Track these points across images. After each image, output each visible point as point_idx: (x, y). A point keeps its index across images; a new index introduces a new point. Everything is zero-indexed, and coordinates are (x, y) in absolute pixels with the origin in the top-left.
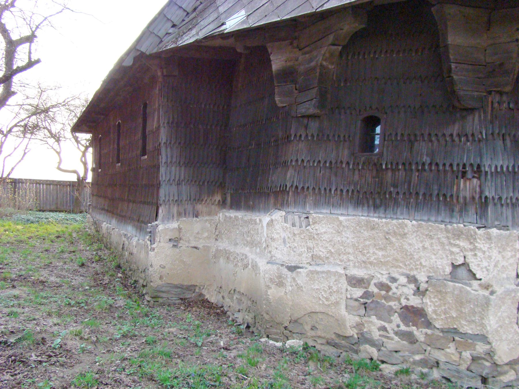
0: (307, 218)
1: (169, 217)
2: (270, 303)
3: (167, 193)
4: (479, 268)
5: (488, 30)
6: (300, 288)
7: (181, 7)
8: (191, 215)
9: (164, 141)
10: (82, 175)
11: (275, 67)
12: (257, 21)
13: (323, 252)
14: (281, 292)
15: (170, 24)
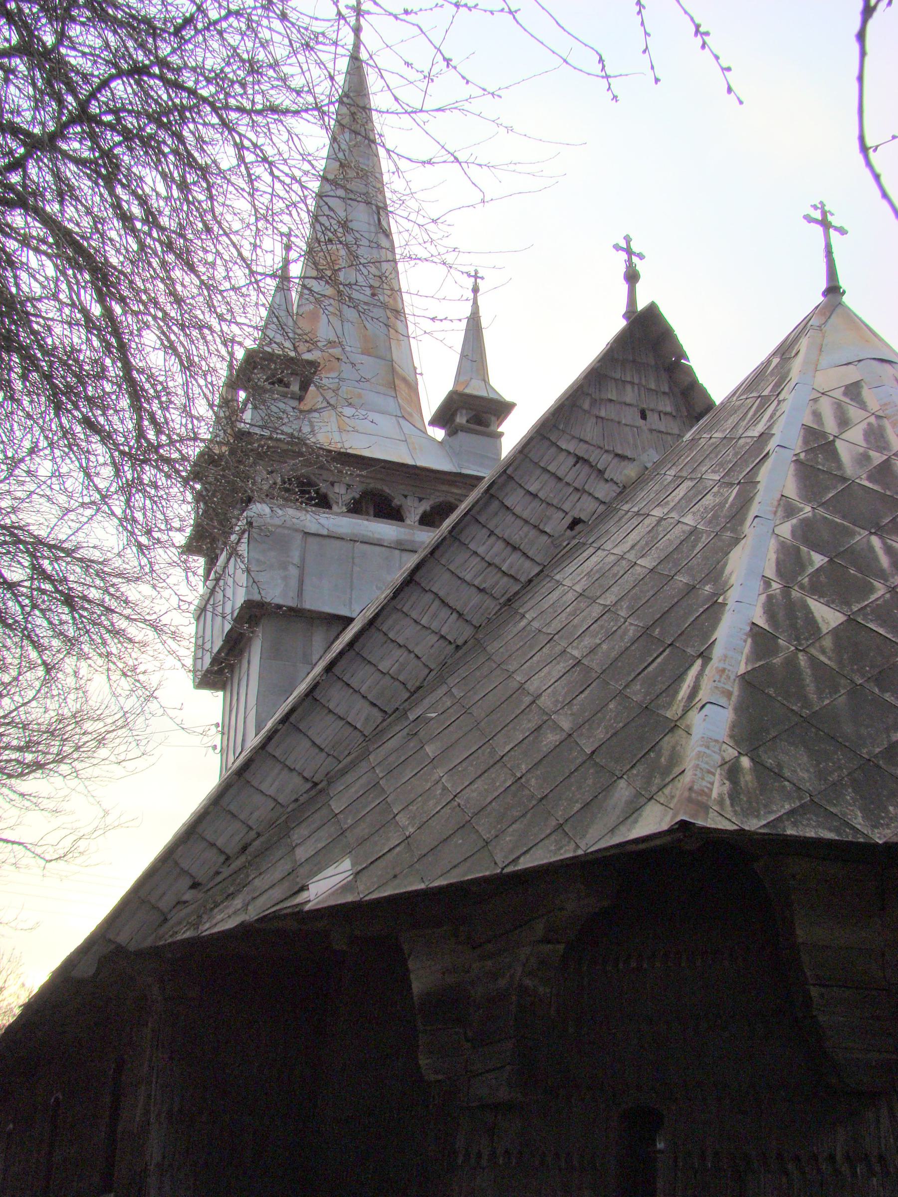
7: (213, 845)
9: (157, 1158)
11: (418, 986)
12: (374, 889)
15: (186, 882)
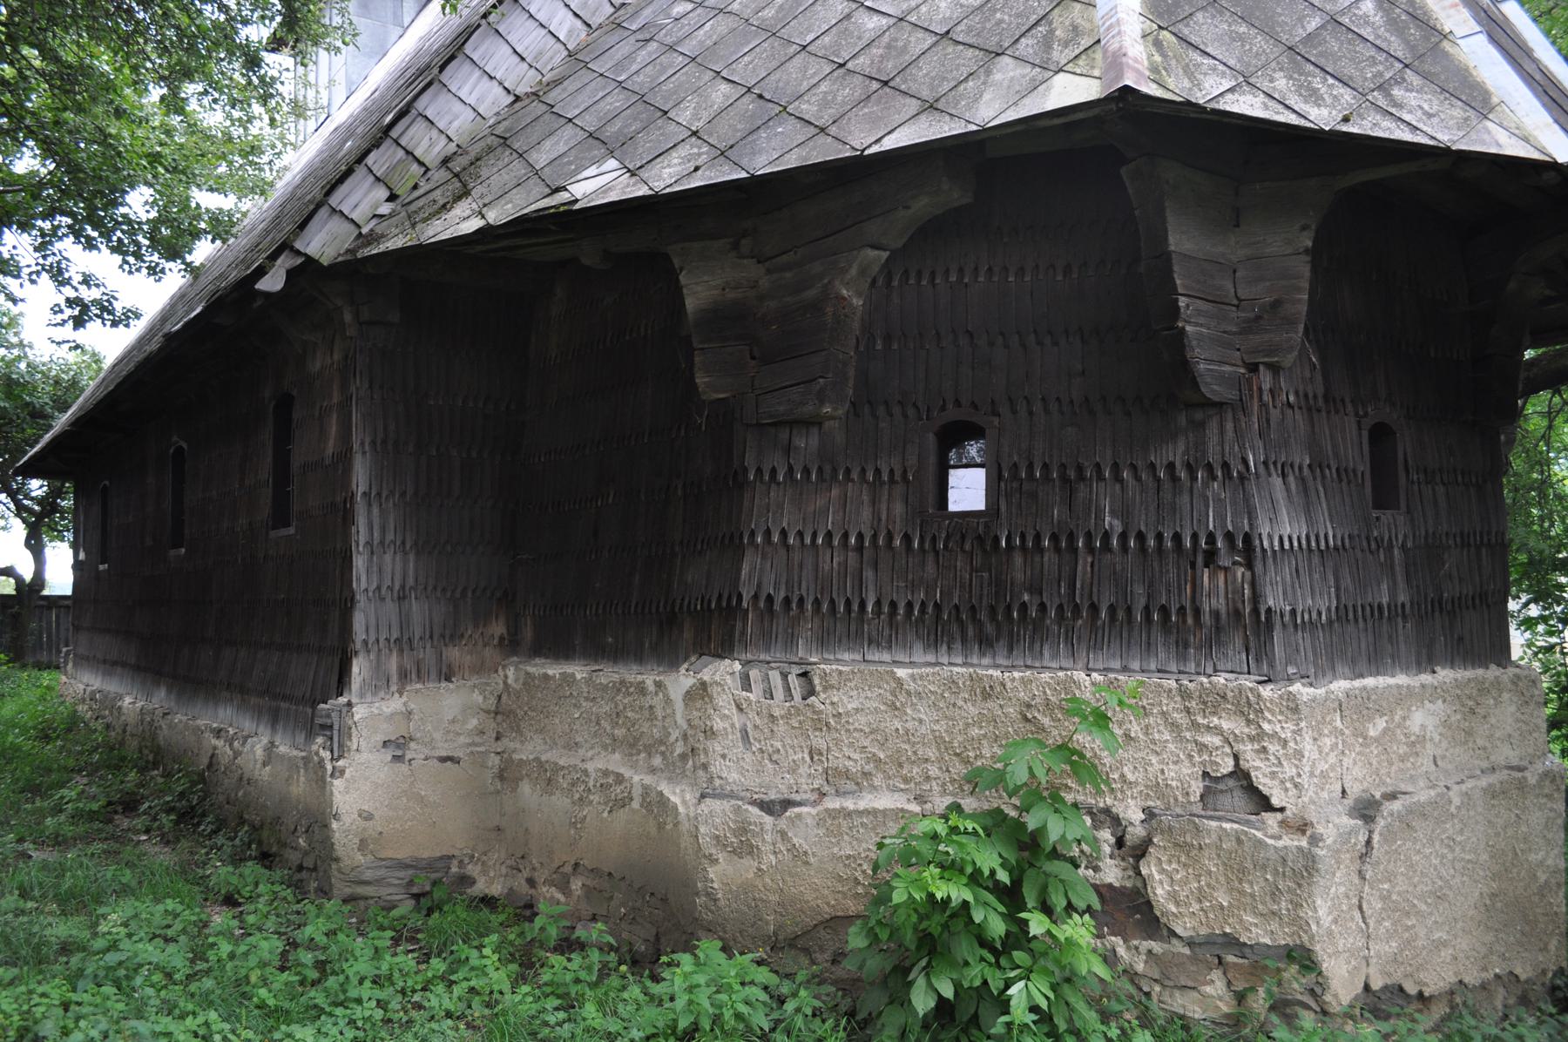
0: (804, 675)
1: (379, 684)
2: (715, 900)
3: (373, 621)
4: (1276, 782)
5: (1237, 226)
6: (798, 855)
8: (433, 675)
10: (28, 575)
11: (691, 304)
13: (856, 761)
14: (746, 868)
15: (383, 193)
